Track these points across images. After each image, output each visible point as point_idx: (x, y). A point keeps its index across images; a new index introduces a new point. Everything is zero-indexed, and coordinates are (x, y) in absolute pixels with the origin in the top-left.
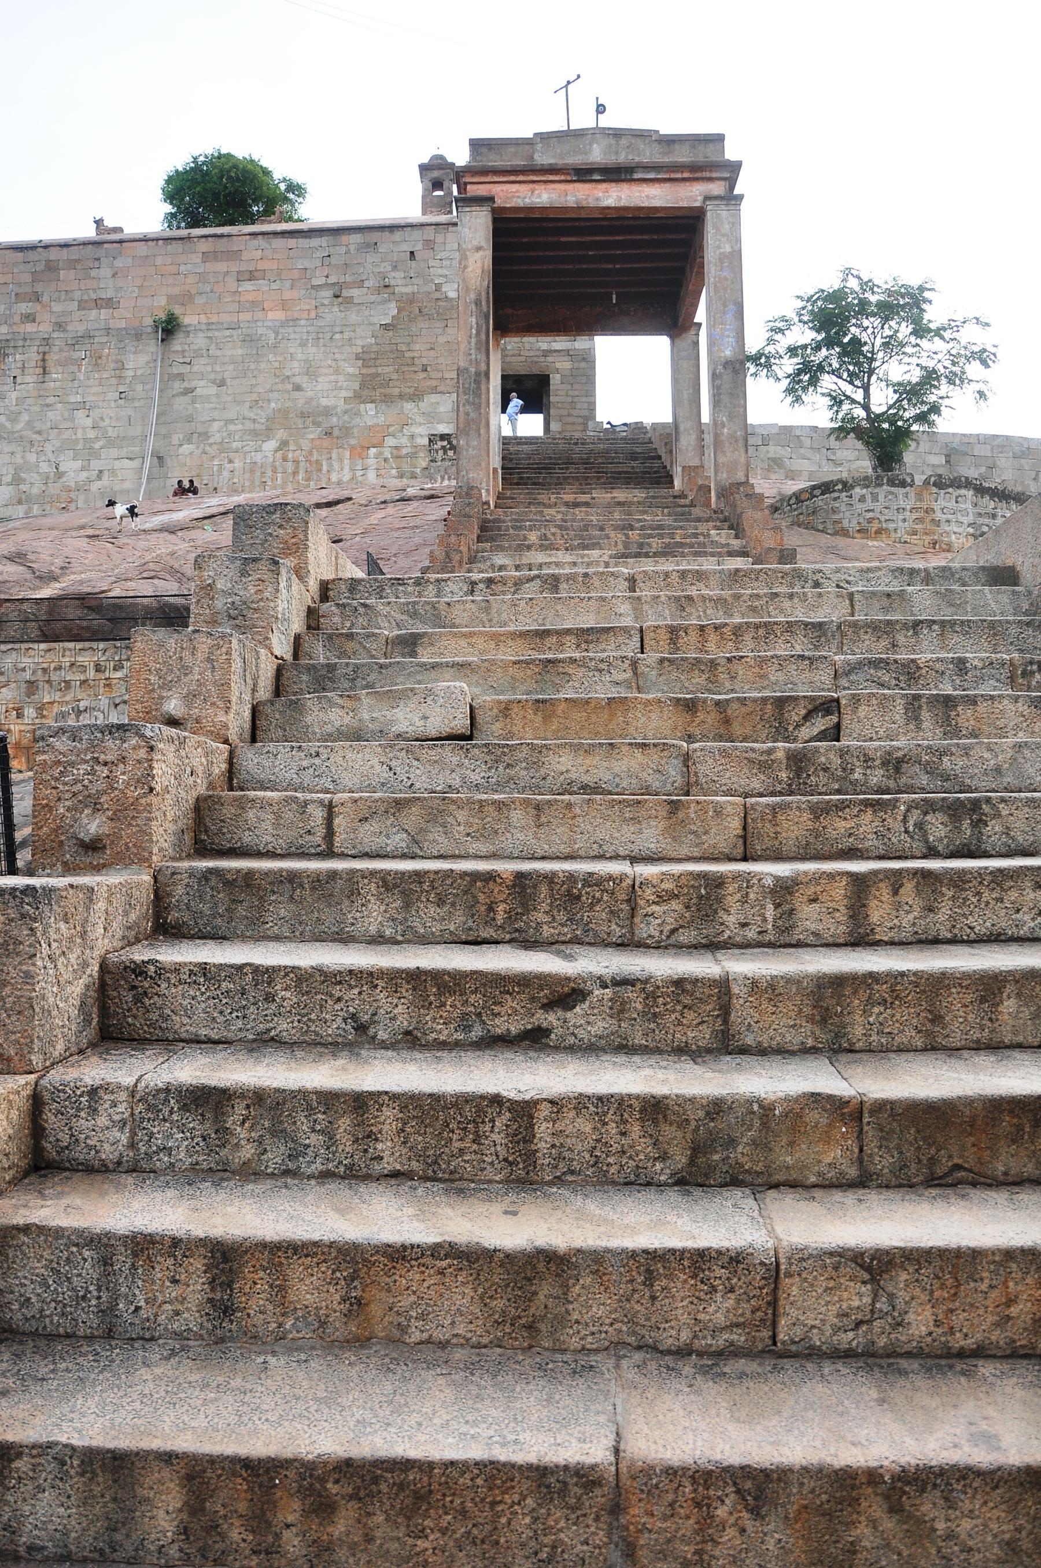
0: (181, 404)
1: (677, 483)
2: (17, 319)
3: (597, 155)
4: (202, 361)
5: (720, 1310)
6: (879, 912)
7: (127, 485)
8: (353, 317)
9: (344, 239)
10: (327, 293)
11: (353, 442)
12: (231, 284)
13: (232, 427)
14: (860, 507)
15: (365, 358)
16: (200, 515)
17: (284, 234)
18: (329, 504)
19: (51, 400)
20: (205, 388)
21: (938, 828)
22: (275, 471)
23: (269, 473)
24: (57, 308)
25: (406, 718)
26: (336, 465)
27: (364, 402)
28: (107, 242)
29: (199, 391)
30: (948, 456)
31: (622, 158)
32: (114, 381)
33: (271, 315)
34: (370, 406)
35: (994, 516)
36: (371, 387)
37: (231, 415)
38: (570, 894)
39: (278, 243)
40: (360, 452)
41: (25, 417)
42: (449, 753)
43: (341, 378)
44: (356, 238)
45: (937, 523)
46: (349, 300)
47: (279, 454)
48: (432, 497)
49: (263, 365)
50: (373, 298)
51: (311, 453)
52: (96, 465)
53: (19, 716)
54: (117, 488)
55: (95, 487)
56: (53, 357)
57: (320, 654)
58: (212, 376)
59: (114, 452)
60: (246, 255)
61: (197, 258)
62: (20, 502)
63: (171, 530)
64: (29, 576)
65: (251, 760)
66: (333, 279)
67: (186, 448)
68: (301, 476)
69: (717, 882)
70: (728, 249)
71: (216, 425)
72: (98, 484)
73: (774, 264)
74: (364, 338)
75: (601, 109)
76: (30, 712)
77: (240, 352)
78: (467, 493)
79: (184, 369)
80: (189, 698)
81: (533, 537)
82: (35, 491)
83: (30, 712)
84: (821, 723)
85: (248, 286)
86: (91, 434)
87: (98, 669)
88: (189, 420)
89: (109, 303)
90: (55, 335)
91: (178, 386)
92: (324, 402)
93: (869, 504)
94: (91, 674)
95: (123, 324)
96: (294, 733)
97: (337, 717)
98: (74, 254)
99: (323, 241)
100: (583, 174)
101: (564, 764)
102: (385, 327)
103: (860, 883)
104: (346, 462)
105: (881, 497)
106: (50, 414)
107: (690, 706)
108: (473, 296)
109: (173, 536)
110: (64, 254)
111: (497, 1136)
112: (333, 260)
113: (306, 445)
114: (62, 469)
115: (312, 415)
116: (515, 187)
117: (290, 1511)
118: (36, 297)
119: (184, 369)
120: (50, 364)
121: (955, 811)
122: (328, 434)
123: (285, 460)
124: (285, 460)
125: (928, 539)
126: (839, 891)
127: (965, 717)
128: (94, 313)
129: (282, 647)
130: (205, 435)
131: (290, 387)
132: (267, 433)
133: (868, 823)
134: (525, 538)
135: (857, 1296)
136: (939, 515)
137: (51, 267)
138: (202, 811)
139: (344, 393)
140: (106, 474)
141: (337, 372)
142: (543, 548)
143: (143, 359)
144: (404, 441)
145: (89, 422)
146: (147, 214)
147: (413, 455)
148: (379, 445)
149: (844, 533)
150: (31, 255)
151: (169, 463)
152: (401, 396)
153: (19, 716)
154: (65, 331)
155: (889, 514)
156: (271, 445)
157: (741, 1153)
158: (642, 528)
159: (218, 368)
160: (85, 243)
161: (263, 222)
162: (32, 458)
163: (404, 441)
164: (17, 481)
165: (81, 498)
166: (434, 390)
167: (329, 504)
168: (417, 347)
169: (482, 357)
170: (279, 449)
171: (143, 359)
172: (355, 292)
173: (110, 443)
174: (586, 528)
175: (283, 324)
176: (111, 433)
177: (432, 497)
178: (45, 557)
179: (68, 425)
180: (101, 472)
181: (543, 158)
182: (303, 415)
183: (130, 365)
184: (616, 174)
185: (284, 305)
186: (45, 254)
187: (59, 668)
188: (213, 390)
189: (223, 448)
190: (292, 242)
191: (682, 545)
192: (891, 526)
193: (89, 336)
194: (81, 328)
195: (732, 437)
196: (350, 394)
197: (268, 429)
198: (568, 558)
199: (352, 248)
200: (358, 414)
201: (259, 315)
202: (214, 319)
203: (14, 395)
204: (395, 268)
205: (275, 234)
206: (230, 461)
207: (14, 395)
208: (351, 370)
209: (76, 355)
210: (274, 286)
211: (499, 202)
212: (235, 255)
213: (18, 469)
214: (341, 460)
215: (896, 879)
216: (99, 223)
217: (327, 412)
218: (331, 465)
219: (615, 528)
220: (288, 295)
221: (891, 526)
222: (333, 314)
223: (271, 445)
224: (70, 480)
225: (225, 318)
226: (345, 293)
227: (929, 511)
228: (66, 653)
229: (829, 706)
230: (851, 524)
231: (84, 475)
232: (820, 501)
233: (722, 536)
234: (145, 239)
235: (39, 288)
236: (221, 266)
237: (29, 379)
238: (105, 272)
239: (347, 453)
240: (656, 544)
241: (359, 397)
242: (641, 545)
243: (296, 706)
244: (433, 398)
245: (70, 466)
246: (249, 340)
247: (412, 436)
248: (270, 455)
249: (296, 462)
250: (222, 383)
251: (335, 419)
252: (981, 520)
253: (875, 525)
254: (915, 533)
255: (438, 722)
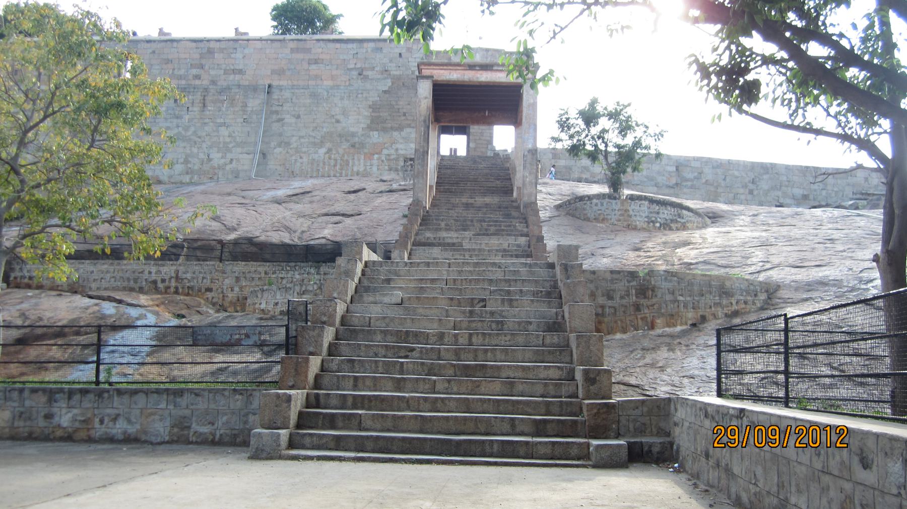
0: (276, 127)
1: (515, 194)
2: (191, 77)
3: (478, 59)
4: (288, 105)
5: (427, 386)
6: (474, 340)
7: (246, 167)
8: (368, 86)
9: (365, 45)
10: (355, 73)
11: (366, 151)
12: (306, 66)
13: (302, 140)
14: (595, 208)
15: (374, 107)
16: (291, 193)
17: (334, 41)
18: (355, 192)
19: (207, 121)
20: (289, 119)
21: (494, 326)
22: (324, 163)
23: (321, 164)
24: (212, 72)
25: (386, 300)
26: (356, 163)
27: (373, 130)
28: (240, 41)
29: (286, 120)
30: (677, 168)
31: (488, 61)
32: (241, 113)
33: (325, 83)
34: (376, 133)
35: (658, 213)
36: (376, 123)
37: (303, 133)
38: (416, 334)
39: (331, 45)
40: (369, 156)
41: (192, 129)
42: (396, 308)
43: (361, 117)
44: (371, 45)
45: (630, 216)
46: (366, 77)
47: (327, 156)
48: (405, 190)
49: (320, 109)
50: (379, 77)
51: (343, 155)
52: (229, 156)
53: (232, 290)
54: (240, 168)
55: (228, 167)
56: (209, 98)
57: (366, 283)
58: (293, 113)
59: (239, 150)
60: (313, 51)
61: (288, 51)
62: (187, 173)
63: (278, 202)
64: (224, 228)
65: (352, 307)
66: (358, 66)
67: (278, 150)
68: (338, 167)
69: (444, 333)
70: (532, 101)
71: (294, 139)
72: (231, 166)
73: (550, 112)
74: (374, 97)
75: (480, 38)
76: (237, 289)
77: (308, 101)
78: (416, 203)
79: (279, 109)
80: (339, 293)
81: (443, 224)
82: (196, 168)
83: (237, 289)
84: (482, 304)
85: (313, 67)
86: (228, 140)
87: (266, 273)
88: (281, 135)
89: (240, 72)
90: (211, 87)
91: (274, 117)
92: (352, 129)
93: (599, 207)
94: (263, 275)
95: (247, 83)
96: (361, 301)
97: (371, 299)
98: (223, 45)
99: (355, 45)
100: (471, 67)
101: (421, 311)
102: (385, 92)
103: (471, 335)
104: (362, 161)
105: (605, 204)
106: (206, 128)
107: (452, 299)
108: (422, 118)
109: (280, 207)
110: (218, 45)
111: (398, 367)
112: (359, 56)
113: (341, 151)
114: (211, 157)
115: (345, 136)
116: (442, 72)
117: (366, 402)
118: (202, 67)
119: (279, 109)
120: (208, 103)
121: (498, 322)
122: (353, 146)
123: (330, 158)
124: (330, 158)
125: (625, 224)
126: (467, 335)
127: (515, 303)
128: (231, 77)
129: (356, 280)
130: (288, 144)
131: (334, 121)
132: (321, 144)
133: (480, 324)
134: (439, 225)
135: (446, 385)
136: (631, 213)
137: (211, 52)
138: (343, 317)
139: (363, 125)
140: (234, 162)
141: (359, 114)
142: (446, 230)
143: (257, 102)
144: (393, 152)
145: (226, 133)
146: (262, 26)
147: (397, 159)
148: (380, 153)
149: (587, 219)
150: (201, 45)
151: (268, 157)
152: (392, 128)
153: (232, 290)
154: (216, 85)
155: (608, 212)
156: (323, 150)
157: (436, 371)
158: (489, 221)
159: (296, 109)
160: (229, 40)
161: (323, 33)
162: (195, 150)
163: (393, 152)
164: (186, 162)
165: (220, 173)
166: (409, 126)
167: (355, 192)
168: (401, 103)
169: (425, 145)
170: (327, 153)
171: (257, 102)
172: (370, 73)
173: (238, 145)
174: (465, 221)
175: (332, 88)
176: (238, 139)
177: (405, 190)
178: (230, 221)
179: (216, 134)
180: (232, 160)
181: (456, 59)
182: (340, 136)
183: (250, 105)
184: (486, 67)
185: (333, 78)
186: (207, 44)
187: (250, 272)
188: (293, 120)
189: (297, 151)
190: (338, 45)
191: (503, 230)
192: (609, 217)
193: (229, 88)
194: (225, 84)
195: (531, 182)
196: (365, 126)
197: (322, 142)
198: (456, 235)
199: (369, 50)
200: (369, 136)
201: (319, 82)
202: (295, 83)
203: (187, 117)
204: (391, 61)
205: (329, 40)
206: (301, 158)
207: (187, 117)
208: (366, 114)
209: (222, 98)
210: (327, 68)
211: (435, 78)
212: (308, 51)
213: (187, 156)
214: (359, 160)
215: (478, 334)
216: (236, 29)
217: (353, 135)
218: (354, 163)
219: (478, 221)
220: (334, 72)
221: (609, 217)
222: (358, 84)
223: (323, 150)
224: (215, 163)
225: (301, 83)
226: (364, 73)
227: (627, 211)
228: (252, 266)
229: (484, 300)
230: (591, 215)
231: (223, 161)
232: (578, 204)
233: (520, 227)
234: (261, 40)
235: (203, 62)
236: (300, 56)
237: (195, 109)
238: (239, 55)
239: (362, 157)
240: (493, 229)
241: (370, 128)
242: (486, 230)
243: (361, 296)
244: (408, 130)
245: (216, 156)
246: (314, 95)
247: (397, 150)
248: (322, 155)
249: (336, 160)
250: (298, 117)
251: (357, 139)
252: (651, 215)
253: (602, 217)
254: (619, 220)
255: (251, 343)
